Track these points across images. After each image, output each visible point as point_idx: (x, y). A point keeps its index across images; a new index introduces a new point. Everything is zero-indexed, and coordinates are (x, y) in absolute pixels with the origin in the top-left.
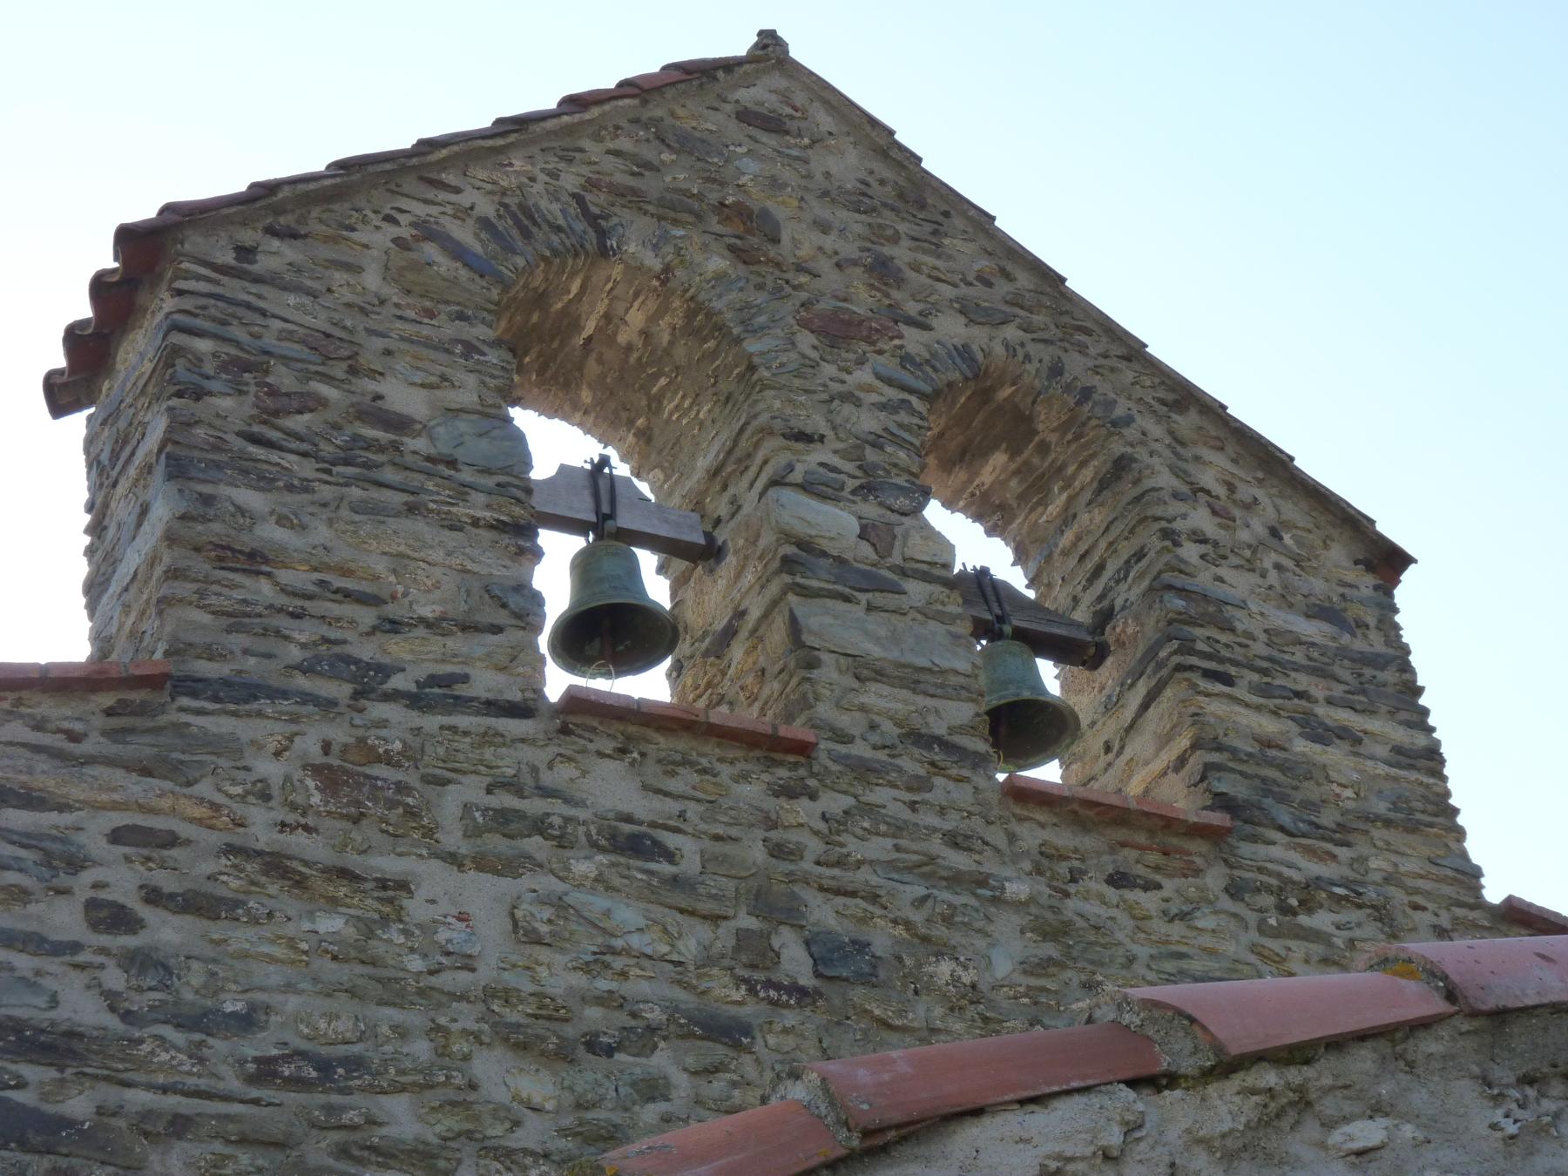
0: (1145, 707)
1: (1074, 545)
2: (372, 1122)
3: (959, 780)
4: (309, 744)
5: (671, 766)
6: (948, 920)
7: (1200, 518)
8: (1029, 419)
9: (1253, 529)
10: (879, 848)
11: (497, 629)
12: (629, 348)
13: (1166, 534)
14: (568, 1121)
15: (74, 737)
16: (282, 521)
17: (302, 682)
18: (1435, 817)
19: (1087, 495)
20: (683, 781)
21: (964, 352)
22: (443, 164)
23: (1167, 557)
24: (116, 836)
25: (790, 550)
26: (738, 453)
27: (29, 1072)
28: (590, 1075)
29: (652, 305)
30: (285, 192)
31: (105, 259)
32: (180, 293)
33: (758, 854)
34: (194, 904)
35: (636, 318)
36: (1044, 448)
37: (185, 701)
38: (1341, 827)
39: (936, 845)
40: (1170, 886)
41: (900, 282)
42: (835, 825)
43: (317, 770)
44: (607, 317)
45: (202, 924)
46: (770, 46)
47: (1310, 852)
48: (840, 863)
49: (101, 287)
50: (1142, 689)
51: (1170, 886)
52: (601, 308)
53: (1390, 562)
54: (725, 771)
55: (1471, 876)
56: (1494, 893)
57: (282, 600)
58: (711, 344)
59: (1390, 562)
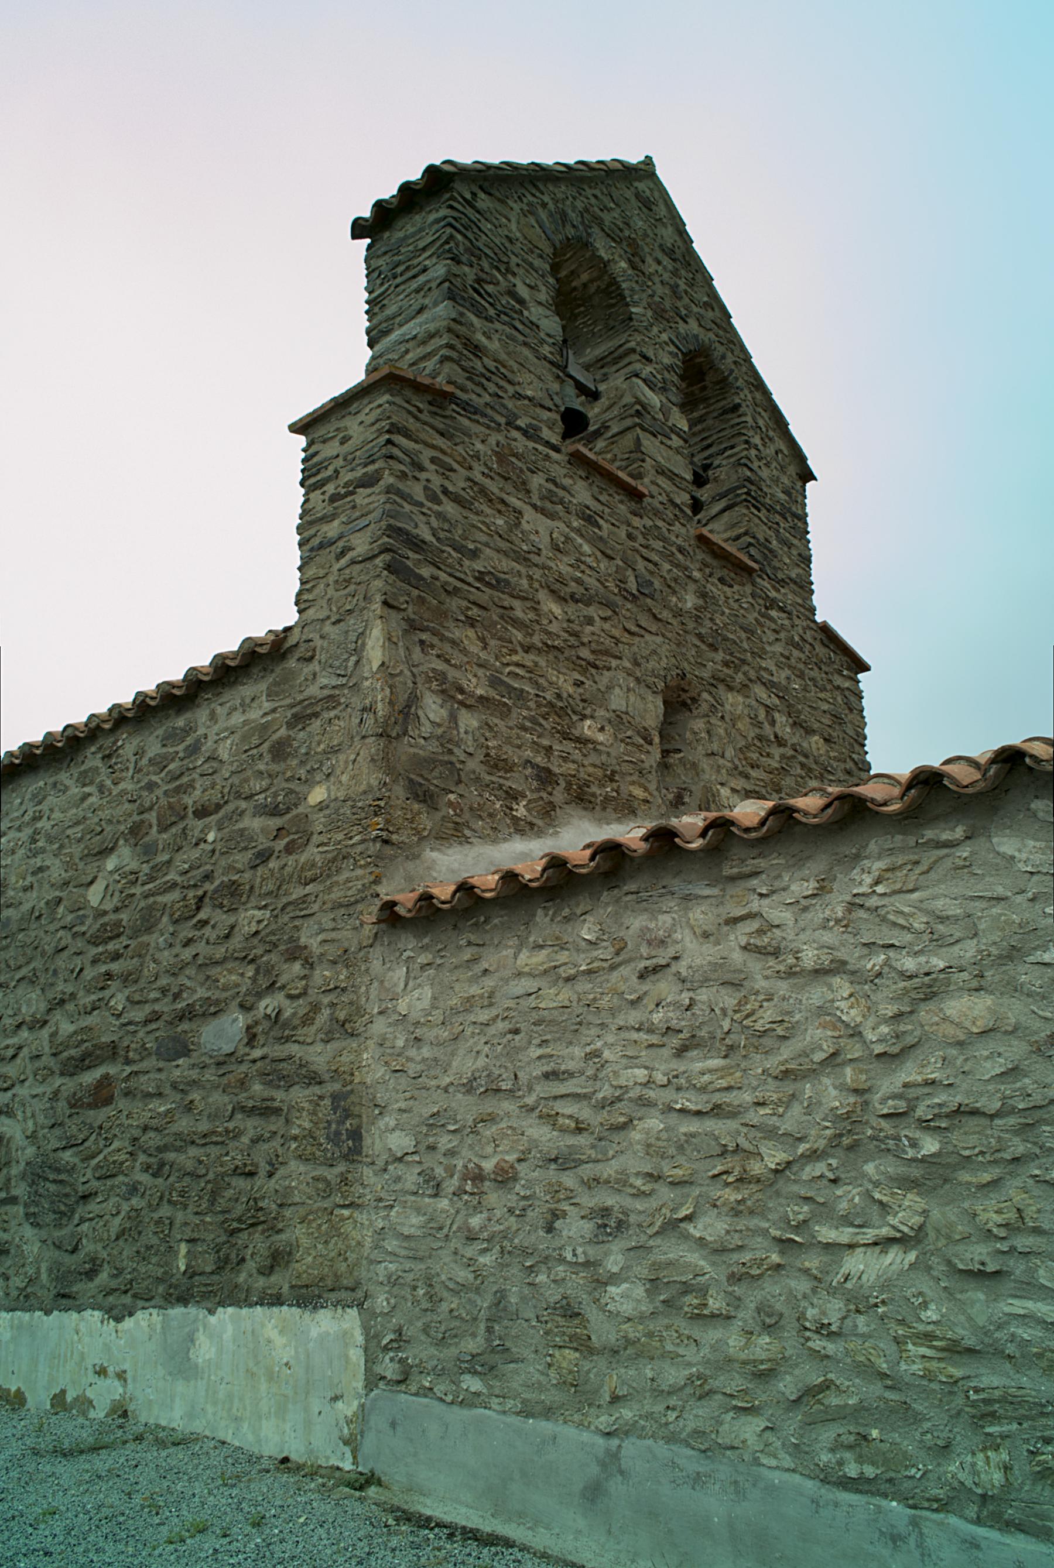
0: (724, 511)
1: (700, 432)
2: (512, 608)
3: (683, 525)
4: (492, 440)
5: (602, 490)
6: (676, 580)
7: (757, 440)
8: (704, 374)
9: (770, 451)
10: (658, 545)
11: (550, 410)
12: (575, 289)
13: (747, 442)
14: (565, 625)
15: (420, 411)
16: (484, 333)
17: (489, 411)
18: (805, 587)
19: (715, 414)
20: (604, 498)
21: (696, 337)
22: (539, 179)
23: (745, 453)
24: (433, 460)
25: (638, 407)
26: (616, 355)
27: (410, 554)
28: (571, 608)
29: (595, 274)
30: (491, 172)
31: (415, 174)
32: (451, 207)
33: (623, 535)
34: (457, 500)
35: (585, 277)
36: (704, 388)
37: (454, 406)
38: (783, 580)
39: (674, 549)
40: (736, 587)
41: (680, 298)
42: (646, 532)
43: (496, 453)
44: (572, 272)
45: (460, 509)
46: (648, 161)
47: (774, 587)
48: (646, 547)
49: (406, 188)
50: (723, 504)
51: (736, 587)
52: (573, 267)
53: (808, 476)
54: (617, 497)
55: (813, 610)
56: (819, 618)
57: (484, 371)
58: (613, 301)
59: (808, 476)
